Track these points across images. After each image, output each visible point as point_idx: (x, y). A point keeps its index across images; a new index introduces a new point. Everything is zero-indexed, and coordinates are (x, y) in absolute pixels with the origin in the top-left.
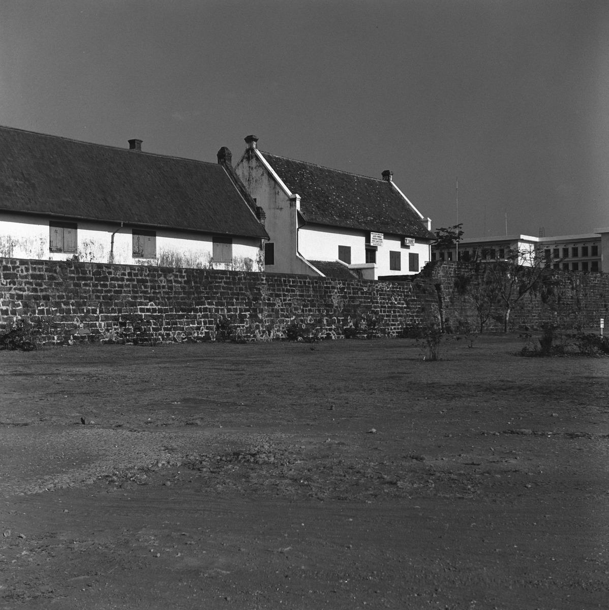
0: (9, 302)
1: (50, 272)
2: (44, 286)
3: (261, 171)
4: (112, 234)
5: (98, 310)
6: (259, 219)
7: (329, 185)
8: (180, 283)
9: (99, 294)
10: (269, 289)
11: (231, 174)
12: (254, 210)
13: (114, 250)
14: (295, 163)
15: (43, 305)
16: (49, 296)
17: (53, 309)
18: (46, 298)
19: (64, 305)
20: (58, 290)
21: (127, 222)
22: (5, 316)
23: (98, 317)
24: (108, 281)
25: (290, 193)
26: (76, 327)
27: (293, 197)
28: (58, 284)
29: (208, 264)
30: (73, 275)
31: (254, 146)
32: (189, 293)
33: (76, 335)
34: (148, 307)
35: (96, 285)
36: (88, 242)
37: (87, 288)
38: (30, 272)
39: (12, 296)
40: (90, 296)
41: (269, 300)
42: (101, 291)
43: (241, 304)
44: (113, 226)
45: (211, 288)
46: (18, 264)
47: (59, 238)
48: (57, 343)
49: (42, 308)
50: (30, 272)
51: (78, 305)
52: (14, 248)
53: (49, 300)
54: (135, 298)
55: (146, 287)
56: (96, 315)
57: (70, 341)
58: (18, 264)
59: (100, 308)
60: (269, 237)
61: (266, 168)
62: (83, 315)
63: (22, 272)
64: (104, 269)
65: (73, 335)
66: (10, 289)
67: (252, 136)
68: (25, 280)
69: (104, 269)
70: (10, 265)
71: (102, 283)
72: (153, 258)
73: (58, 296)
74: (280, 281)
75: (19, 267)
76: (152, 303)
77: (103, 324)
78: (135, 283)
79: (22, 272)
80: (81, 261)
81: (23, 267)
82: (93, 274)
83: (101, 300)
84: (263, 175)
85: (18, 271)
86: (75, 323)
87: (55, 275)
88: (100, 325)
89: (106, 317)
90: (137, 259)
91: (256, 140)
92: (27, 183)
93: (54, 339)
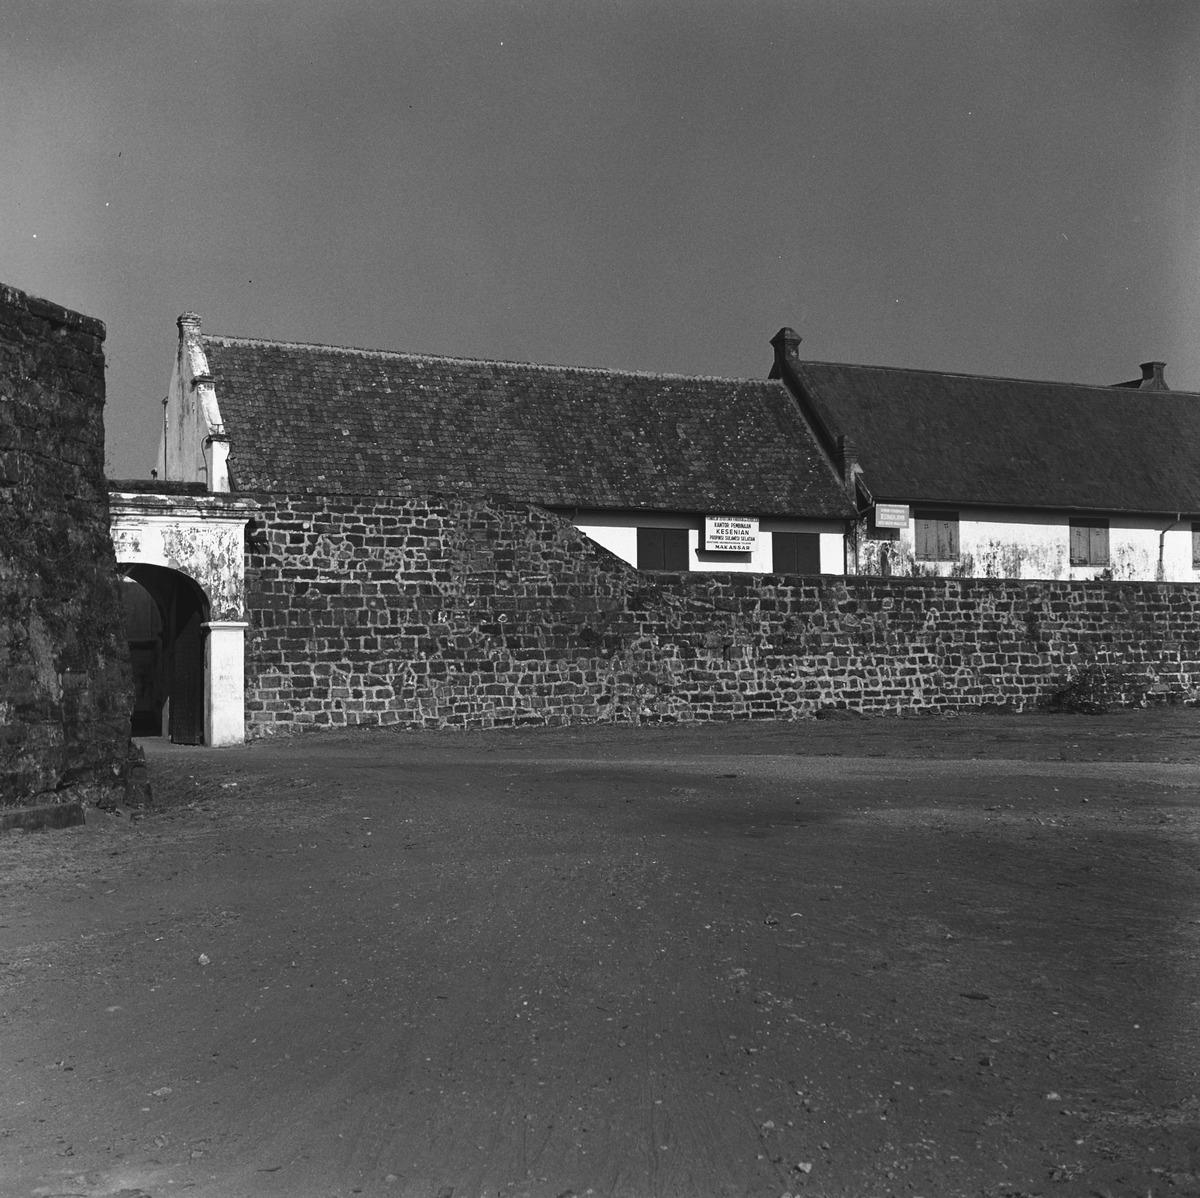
0: (1061, 644)
1: (1111, 599)
2: (1104, 621)
4: (1161, 532)
5: (1179, 655)
9: (1179, 631)
13: (1164, 558)
15: (1103, 649)
16: (1111, 635)
17: (1118, 654)
18: (1107, 638)
19: (1133, 648)
21: (1186, 513)
22: (1057, 666)
23: (1179, 666)
24: (1190, 610)
26: (1150, 681)
28: (1122, 617)
30: (1141, 603)
33: (1150, 692)
35: (1173, 618)
36: (1126, 548)
37: (1163, 622)
38: (1086, 600)
39: (1064, 636)
40: (1166, 634)
42: (1181, 627)
44: (1162, 520)
46: (1069, 590)
47: (1084, 543)
48: (1126, 705)
49: (1103, 652)
50: (1086, 600)
51: (1151, 647)
52: (1022, 562)
53: (1111, 641)
56: (1175, 663)
57: (1142, 702)
58: (1069, 590)
59: (1182, 651)
62: (1158, 662)
63: (1075, 601)
64: (1185, 592)
65: (1146, 693)
66: (1061, 626)
68: (1078, 612)
69: (1185, 592)
70: (1059, 592)
71: (1182, 613)
73: (1123, 635)
75: (1070, 594)
77: (1186, 675)
79: (1075, 601)
80: (1116, 578)
81: (1076, 593)
82: (1170, 601)
83: (1183, 640)
85: (1069, 600)
86: (1148, 674)
87: (1117, 603)
88: (1183, 677)
89: (1190, 665)
92: (1035, 462)
93: (1121, 699)
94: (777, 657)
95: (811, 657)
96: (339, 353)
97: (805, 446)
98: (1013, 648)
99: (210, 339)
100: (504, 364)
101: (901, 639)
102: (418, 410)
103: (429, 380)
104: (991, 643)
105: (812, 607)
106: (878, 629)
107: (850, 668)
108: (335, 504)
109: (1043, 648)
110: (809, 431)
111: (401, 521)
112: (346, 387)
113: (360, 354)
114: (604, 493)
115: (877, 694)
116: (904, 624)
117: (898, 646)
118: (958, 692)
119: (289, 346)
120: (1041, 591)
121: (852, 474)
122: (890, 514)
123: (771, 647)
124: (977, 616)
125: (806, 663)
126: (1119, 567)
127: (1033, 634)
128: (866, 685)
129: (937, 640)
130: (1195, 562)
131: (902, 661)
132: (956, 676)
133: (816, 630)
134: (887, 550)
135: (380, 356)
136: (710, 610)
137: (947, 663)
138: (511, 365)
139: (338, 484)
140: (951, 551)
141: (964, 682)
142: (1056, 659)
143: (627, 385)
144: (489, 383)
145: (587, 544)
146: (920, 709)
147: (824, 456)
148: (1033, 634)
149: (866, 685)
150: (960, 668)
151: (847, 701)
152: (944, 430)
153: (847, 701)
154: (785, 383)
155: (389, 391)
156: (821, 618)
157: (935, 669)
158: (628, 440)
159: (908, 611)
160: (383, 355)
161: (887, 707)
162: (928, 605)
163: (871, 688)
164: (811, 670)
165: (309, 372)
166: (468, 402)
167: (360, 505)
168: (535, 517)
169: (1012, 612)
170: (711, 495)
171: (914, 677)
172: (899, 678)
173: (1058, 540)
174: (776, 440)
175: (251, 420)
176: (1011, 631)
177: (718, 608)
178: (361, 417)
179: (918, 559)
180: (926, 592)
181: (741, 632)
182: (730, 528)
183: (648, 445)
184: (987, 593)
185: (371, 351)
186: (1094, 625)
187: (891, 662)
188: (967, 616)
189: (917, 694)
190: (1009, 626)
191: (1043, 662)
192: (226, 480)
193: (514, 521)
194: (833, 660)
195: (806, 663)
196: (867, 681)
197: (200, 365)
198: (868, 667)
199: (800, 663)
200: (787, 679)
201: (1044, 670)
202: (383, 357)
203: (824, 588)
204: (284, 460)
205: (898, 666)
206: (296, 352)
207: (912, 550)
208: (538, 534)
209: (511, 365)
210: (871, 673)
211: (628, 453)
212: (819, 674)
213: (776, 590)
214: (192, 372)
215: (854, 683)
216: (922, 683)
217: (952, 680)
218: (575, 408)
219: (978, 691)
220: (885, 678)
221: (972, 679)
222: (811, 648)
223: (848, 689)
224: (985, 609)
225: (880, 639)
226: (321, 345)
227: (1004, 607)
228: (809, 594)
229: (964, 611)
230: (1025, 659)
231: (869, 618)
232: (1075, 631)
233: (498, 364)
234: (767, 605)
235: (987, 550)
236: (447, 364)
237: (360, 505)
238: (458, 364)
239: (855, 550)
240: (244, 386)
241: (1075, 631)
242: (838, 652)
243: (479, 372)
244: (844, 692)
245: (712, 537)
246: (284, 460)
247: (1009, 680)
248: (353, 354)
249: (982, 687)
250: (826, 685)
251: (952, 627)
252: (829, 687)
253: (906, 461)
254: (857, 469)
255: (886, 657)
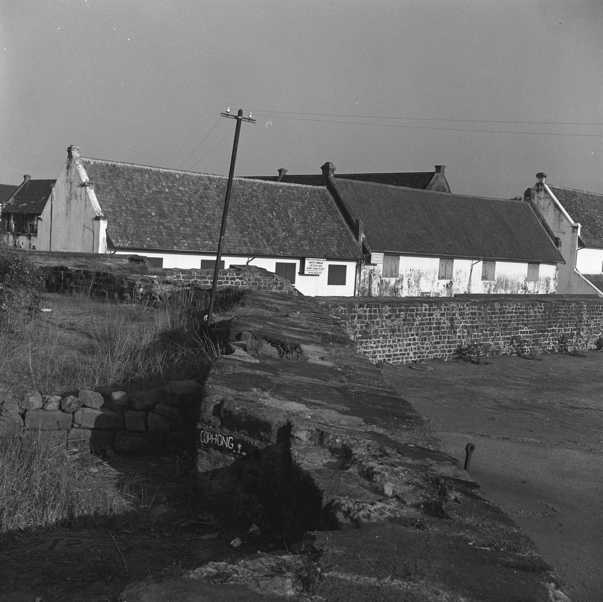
3: (548, 201)
6: (558, 246)
7: (594, 209)
8: (541, 313)
10: (587, 314)
11: (535, 209)
12: (553, 240)
13: (472, 276)
14: (568, 191)
18: (477, 327)
20: (482, 321)
25: (572, 222)
27: (575, 225)
29: (524, 283)
31: (544, 182)
32: (545, 320)
34: (524, 330)
35: (499, 318)
41: (587, 322)
43: (572, 325)
45: (556, 316)
51: (492, 330)
54: (518, 324)
55: (523, 317)
60: (565, 262)
61: (553, 200)
67: (542, 173)
70: (462, 307)
72: (492, 280)
74: (594, 307)
76: (526, 327)
77: (502, 342)
78: (518, 314)
84: (549, 204)
86: (490, 342)
89: (504, 338)
90: (484, 281)
91: (545, 177)
94: (363, 340)
95: (374, 340)
96: (142, 168)
97: (339, 222)
98: (445, 333)
99: (84, 159)
100: (212, 176)
101: (407, 331)
102: (181, 201)
103: (183, 185)
104: (438, 331)
105: (376, 317)
106: (399, 326)
107: (388, 344)
108: (199, 275)
109: (455, 332)
110: (340, 214)
111: (225, 282)
112: (149, 188)
113: (151, 169)
114: (266, 247)
115: (397, 355)
116: (408, 324)
117: (405, 334)
118: (425, 352)
119: (119, 164)
120: (456, 307)
121: (362, 238)
122: (377, 257)
123: (360, 336)
124: (433, 319)
125: (373, 343)
126: (455, 280)
127: (452, 327)
128: (394, 352)
129: (419, 330)
130: (482, 277)
131: (406, 340)
132: (424, 346)
133: (376, 327)
134: (372, 272)
135: (159, 171)
136: (339, 320)
137: (422, 340)
138: (215, 176)
139: (156, 243)
140: (396, 273)
141: (427, 348)
142: (459, 337)
143: (265, 188)
144: (208, 186)
145: (295, 291)
146: (412, 361)
147: (347, 227)
148: (452, 327)
149: (394, 352)
150: (426, 342)
151: (387, 359)
152: (392, 215)
153: (387, 359)
154: (327, 188)
155: (167, 190)
156: (378, 322)
157: (417, 343)
158: (269, 218)
159: (410, 318)
160: (161, 170)
161: (401, 361)
162: (417, 315)
163: (395, 353)
164: (374, 346)
165: (131, 179)
166: (201, 197)
167: (209, 276)
168: (277, 280)
169: (445, 317)
170: (307, 248)
171: (410, 347)
172: (405, 348)
173: (435, 268)
174: (328, 219)
175: (111, 206)
176: (445, 325)
177: (342, 319)
178: (158, 205)
179: (383, 276)
180: (416, 309)
181: (350, 329)
182: (315, 264)
183: (278, 221)
184: (437, 308)
185: (155, 168)
186: (473, 321)
187: (402, 340)
188: (430, 319)
189: (411, 355)
190: (444, 323)
191: (455, 338)
192: (106, 239)
193: (268, 281)
194: (382, 341)
195: (373, 343)
196: (394, 349)
197: (85, 178)
198: (395, 343)
199: (371, 343)
200: (366, 350)
201: (455, 342)
202: (161, 171)
203: (380, 308)
204: (131, 230)
205: (405, 342)
206: (124, 168)
207: (381, 273)
208: (277, 287)
209: (215, 176)
210: (395, 346)
211: (272, 226)
212: (377, 347)
213: (363, 310)
214: (81, 179)
215: (389, 351)
216: (413, 350)
217: (423, 348)
218: (246, 201)
219: (432, 352)
220: (400, 348)
221: (430, 347)
222: (375, 336)
223: (387, 354)
224: (436, 316)
225: (399, 330)
226: (133, 164)
227: (443, 315)
228: (375, 311)
229: (429, 317)
230: (449, 338)
231: (396, 321)
232: (466, 324)
233: (210, 176)
234: (360, 317)
235: (409, 272)
236: (189, 176)
237: (209, 276)
238: (193, 175)
239: (360, 273)
240: (104, 187)
241: (466, 324)
242: (384, 337)
243: (203, 180)
244: (386, 355)
245: (307, 268)
246: (131, 230)
247: (443, 347)
248: (148, 169)
249: (433, 350)
250: (379, 352)
251: (424, 324)
252: (380, 353)
253: (381, 231)
254: (363, 236)
255: (401, 338)
